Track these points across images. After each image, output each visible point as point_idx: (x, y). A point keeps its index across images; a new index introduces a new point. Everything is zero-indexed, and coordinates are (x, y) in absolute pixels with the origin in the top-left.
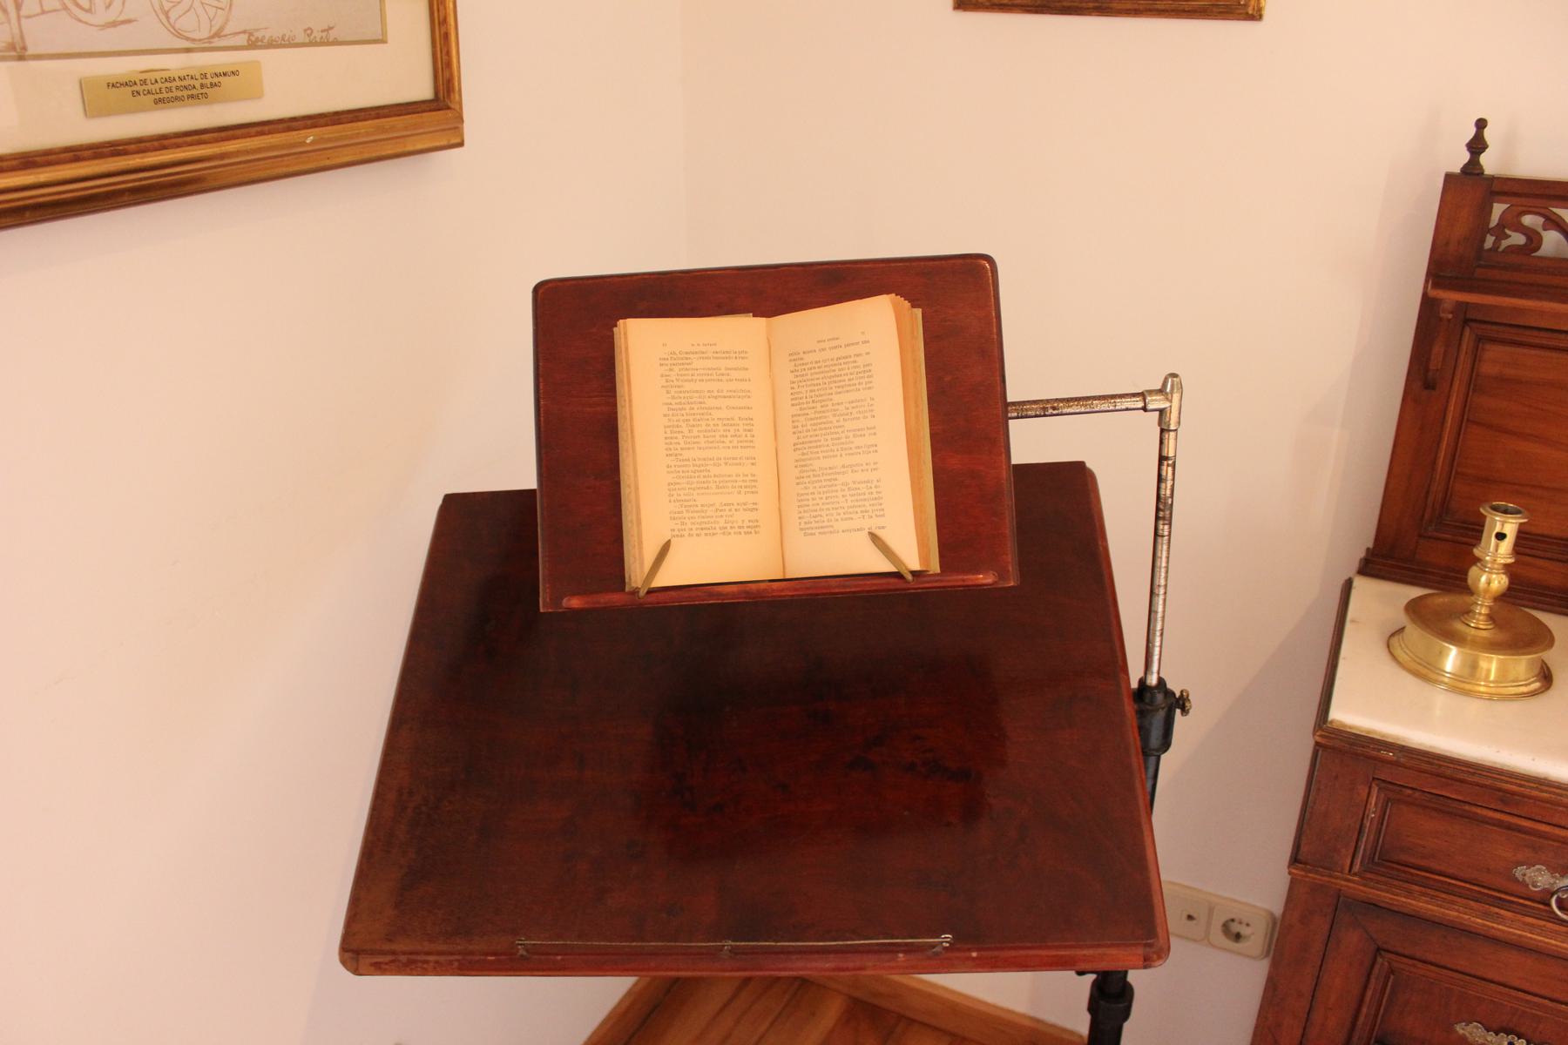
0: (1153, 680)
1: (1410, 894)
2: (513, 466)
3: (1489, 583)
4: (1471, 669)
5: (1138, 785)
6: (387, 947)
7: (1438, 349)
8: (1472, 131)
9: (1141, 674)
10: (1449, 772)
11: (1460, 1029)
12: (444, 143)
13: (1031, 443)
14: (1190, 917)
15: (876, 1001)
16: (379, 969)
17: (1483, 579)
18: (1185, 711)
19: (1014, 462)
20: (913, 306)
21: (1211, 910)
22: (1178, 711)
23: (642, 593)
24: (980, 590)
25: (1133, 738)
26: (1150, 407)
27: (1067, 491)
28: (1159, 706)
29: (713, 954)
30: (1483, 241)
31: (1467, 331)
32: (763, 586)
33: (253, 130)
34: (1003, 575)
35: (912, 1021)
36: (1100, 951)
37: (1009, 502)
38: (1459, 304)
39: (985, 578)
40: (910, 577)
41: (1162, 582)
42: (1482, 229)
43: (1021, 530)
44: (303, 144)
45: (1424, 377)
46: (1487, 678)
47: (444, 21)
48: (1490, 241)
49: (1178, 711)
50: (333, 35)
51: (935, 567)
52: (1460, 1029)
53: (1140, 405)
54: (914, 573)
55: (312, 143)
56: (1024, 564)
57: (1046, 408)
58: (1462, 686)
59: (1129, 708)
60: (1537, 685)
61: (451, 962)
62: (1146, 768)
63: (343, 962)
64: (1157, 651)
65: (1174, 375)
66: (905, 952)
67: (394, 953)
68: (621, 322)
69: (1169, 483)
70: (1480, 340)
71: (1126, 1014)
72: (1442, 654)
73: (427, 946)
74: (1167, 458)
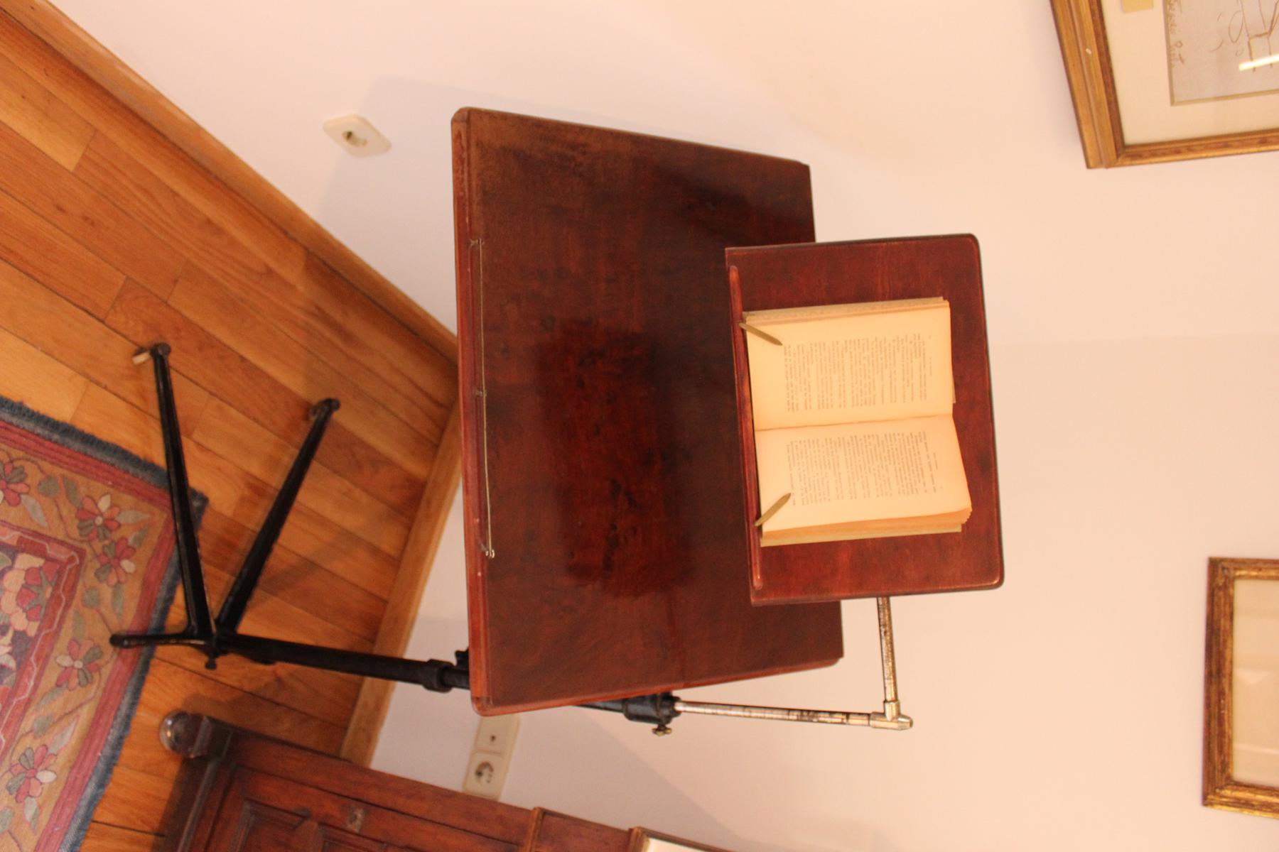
0: (679, 707)
2: (831, 225)
5: (599, 695)
6: (473, 142)
9: (683, 698)
12: (1090, 153)
13: (857, 615)
14: (493, 738)
15: (423, 504)
16: (457, 138)
18: (656, 731)
19: (845, 604)
20: (963, 526)
21: (499, 754)
22: (655, 726)
23: (742, 325)
24: (747, 577)
26: (887, 705)
27: (823, 645)
28: (659, 711)
29: (475, 383)
32: (749, 415)
33: (1095, 7)
34: (761, 593)
35: (409, 529)
37: (814, 598)
39: (757, 580)
40: (757, 524)
43: (790, 609)
44: (1085, 46)
47: (1190, 150)
49: (655, 726)
50: (1177, 64)
51: (765, 543)
53: (889, 698)
54: (760, 528)
55: (1086, 54)
56: (766, 609)
57: (885, 626)
59: (658, 689)
61: (462, 190)
62: (613, 702)
63: (461, 111)
65: (911, 724)
66: (480, 524)
67: (469, 147)
68: (947, 303)
69: (828, 720)
71: (429, 687)
73: (474, 173)
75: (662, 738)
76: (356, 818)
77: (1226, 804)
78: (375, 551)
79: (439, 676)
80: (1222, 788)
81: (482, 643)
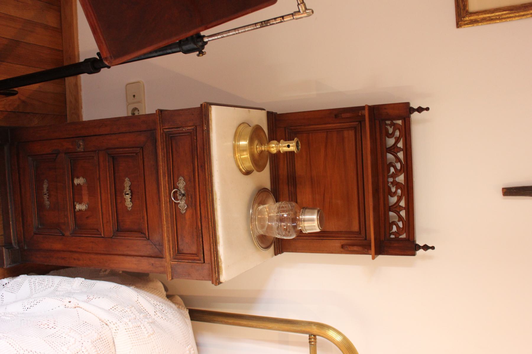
1: (162, 149)
3: (272, 147)
4: (242, 150)
7: (348, 115)
8: (425, 107)
9: (206, 35)
10: (205, 147)
11: (127, 179)
14: (134, 96)
17: (273, 145)
18: (198, 55)
21: (139, 102)
22: (198, 53)
25: (183, 36)
28: (196, 45)
30: (388, 120)
31: (357, 123)
35: (60, 11)
36: (103, 41)
38: (365, 116)
41: (240, 31)
42: (392, 119)
45: (338, 114)
46: (240, 156)
48: (388, 122)
49: (198, 53)
52: (127, 179)
53: (299, 3)
58: (236, 149)
59: (192, 33)
60: (244, 171)
64: (216, 37)
65: (313, 12)
70: (355, 128)
71: (90, 73)
72: (245, 140)
74: (283, 19)
75: (202, 58)
76: (80, 145)
77: (467, 24)
78: (46, 27)
79: (94, 66)
80: (464, 17)
81: (98, 30)
